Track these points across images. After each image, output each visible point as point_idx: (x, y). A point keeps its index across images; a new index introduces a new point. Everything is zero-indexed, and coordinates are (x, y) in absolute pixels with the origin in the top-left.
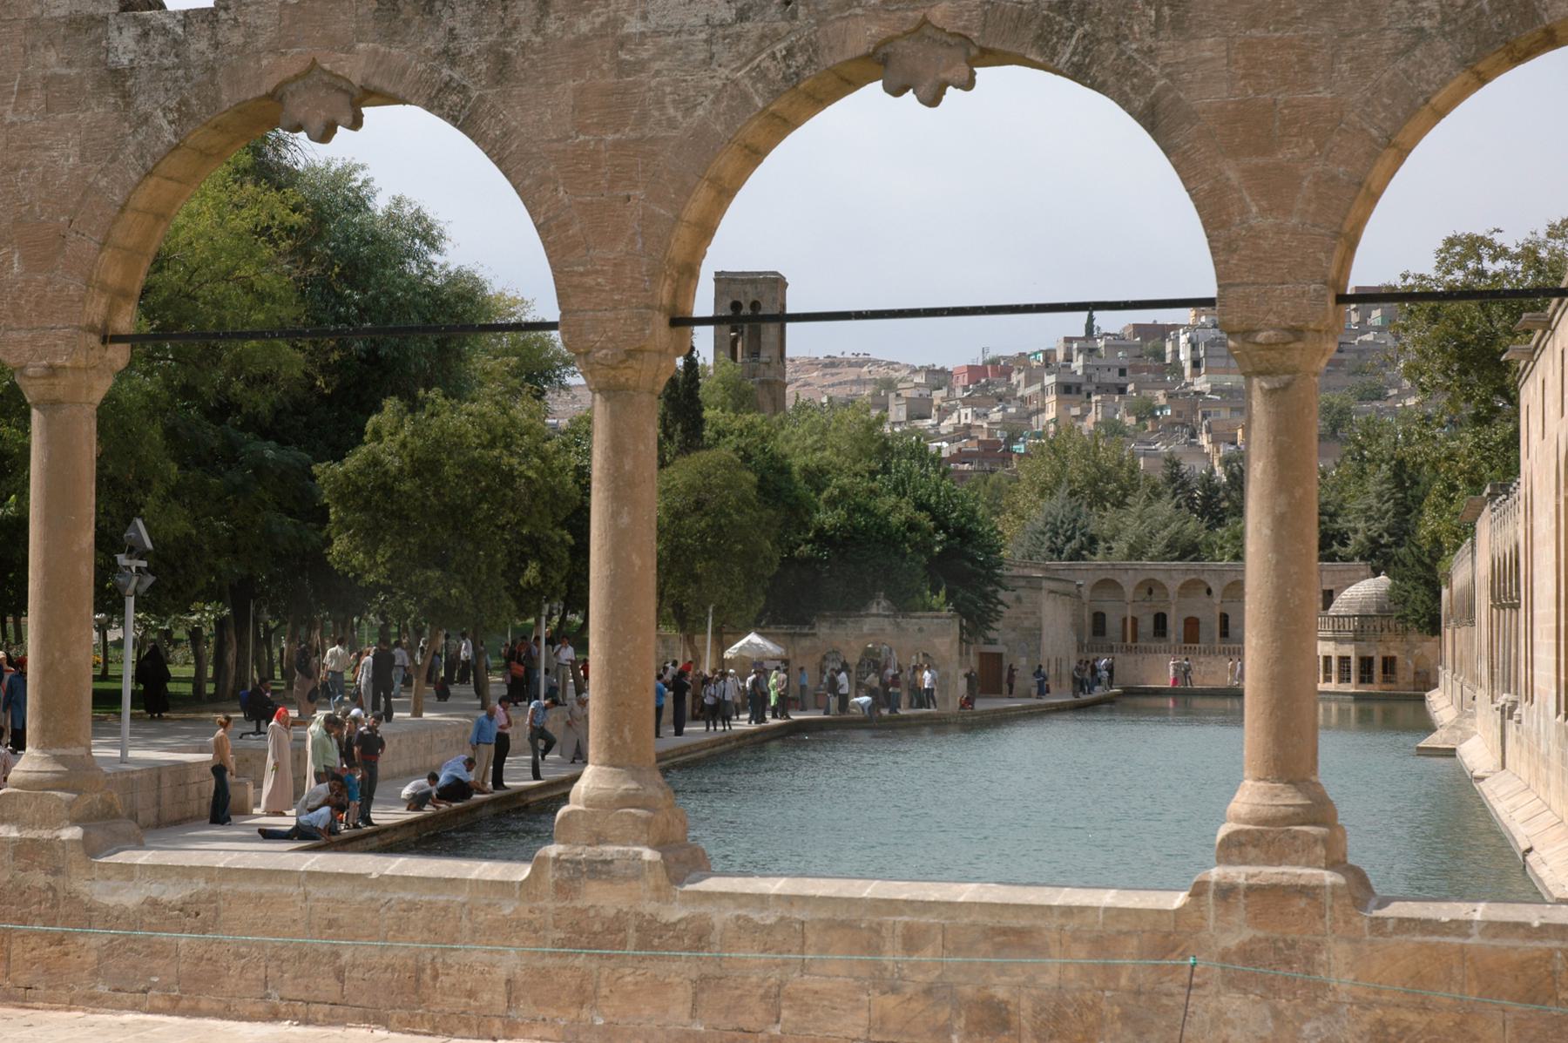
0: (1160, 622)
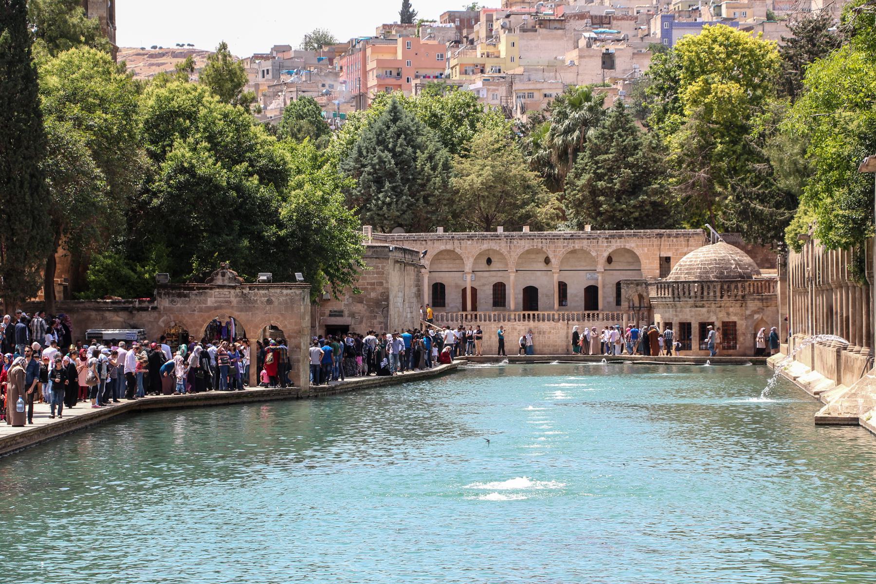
0: (499, 293)
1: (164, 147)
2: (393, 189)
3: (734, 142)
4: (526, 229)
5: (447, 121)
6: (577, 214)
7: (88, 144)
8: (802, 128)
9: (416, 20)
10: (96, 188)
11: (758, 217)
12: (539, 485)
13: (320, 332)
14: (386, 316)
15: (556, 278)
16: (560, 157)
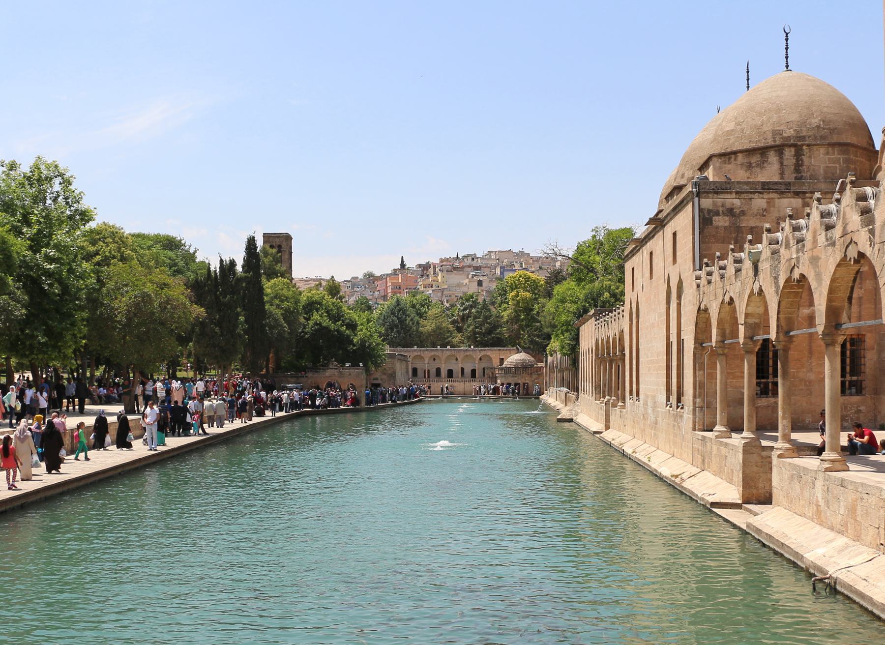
0: (438, 371)
1: (310, 315)
2: (397, 331)
3: (528, 315)
4: (448, 347)
5: (418, 306)
6: (468, 341)
7: (282, 314)
8: (552, 310)
9: (406, 267)
10: (284, 331)
11: (537, 343)
12: (453, 444)
13: (369, 386)
14: (395, 380)
15: (460, 366)
16: (461, 320)
